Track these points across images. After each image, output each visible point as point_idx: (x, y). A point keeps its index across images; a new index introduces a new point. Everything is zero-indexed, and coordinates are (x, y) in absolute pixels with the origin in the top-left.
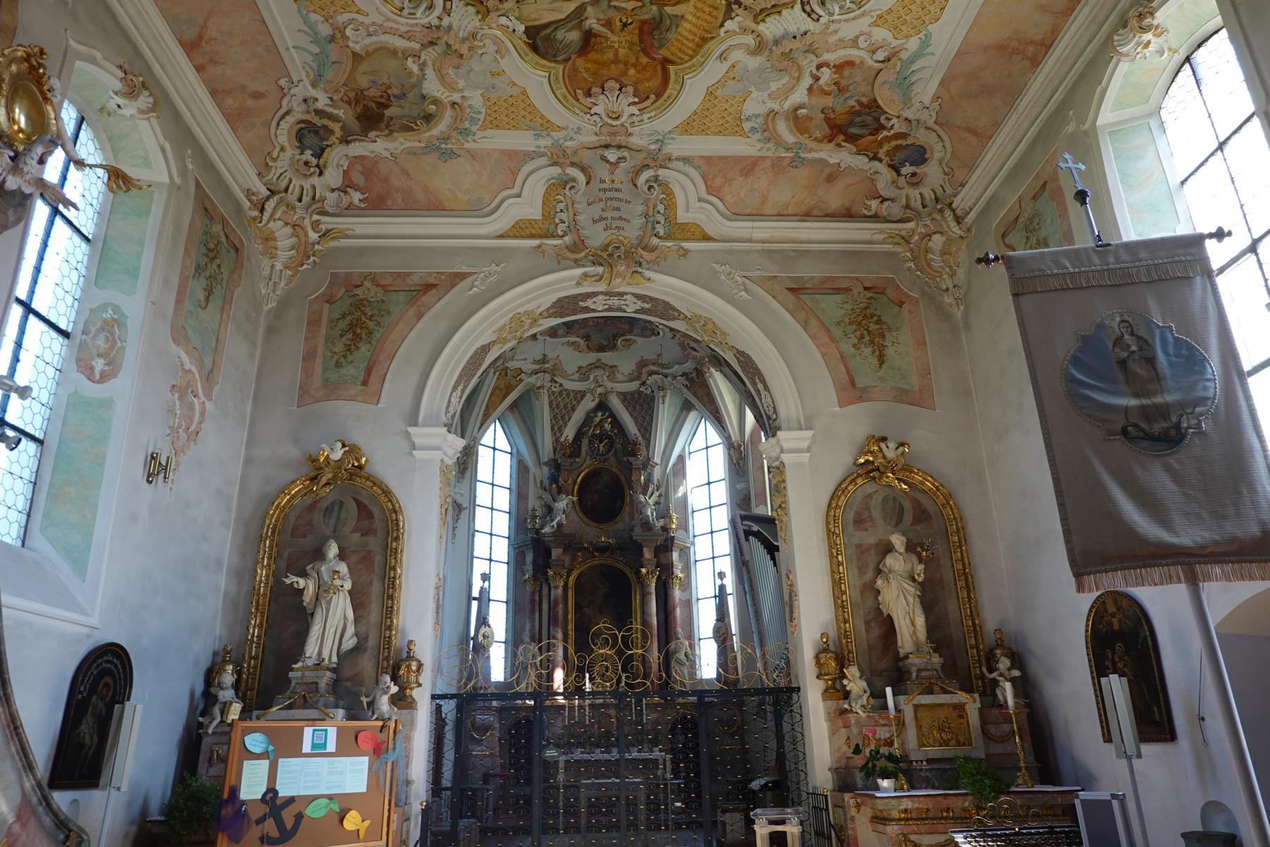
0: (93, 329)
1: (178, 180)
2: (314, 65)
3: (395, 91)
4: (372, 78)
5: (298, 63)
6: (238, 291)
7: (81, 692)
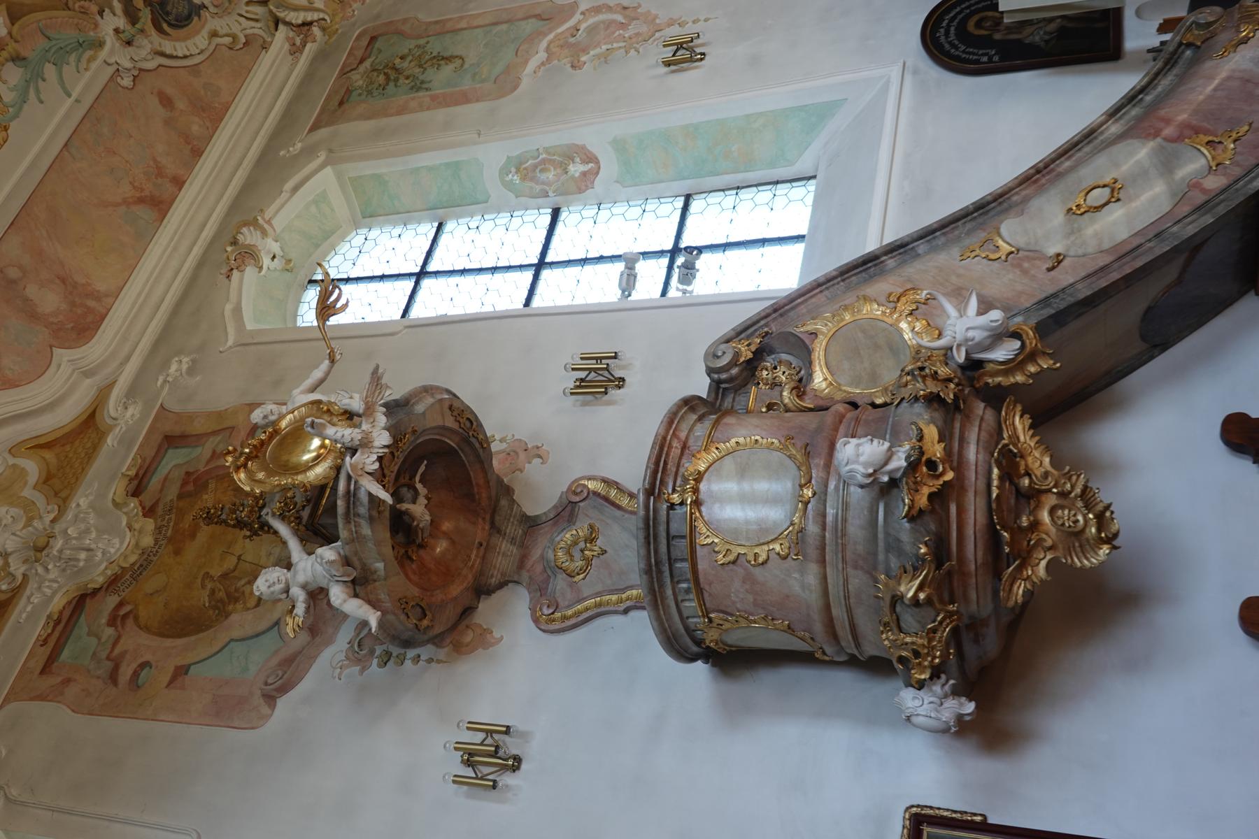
0: (538, 188)
1: (322, 156)
2: (72, 58)
5: (87, 80)
6: (423, 17)
7: (990, 60)
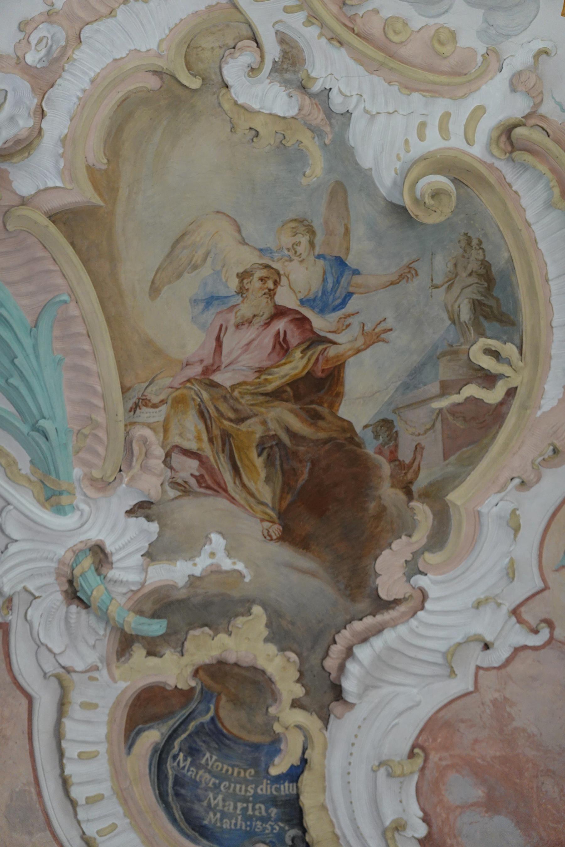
3: (302, 279)
4: (190, 286)
